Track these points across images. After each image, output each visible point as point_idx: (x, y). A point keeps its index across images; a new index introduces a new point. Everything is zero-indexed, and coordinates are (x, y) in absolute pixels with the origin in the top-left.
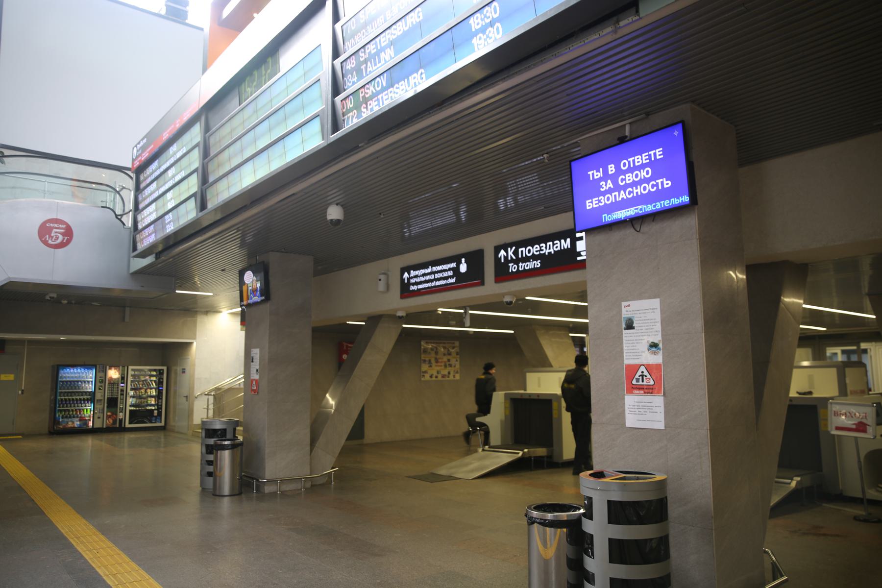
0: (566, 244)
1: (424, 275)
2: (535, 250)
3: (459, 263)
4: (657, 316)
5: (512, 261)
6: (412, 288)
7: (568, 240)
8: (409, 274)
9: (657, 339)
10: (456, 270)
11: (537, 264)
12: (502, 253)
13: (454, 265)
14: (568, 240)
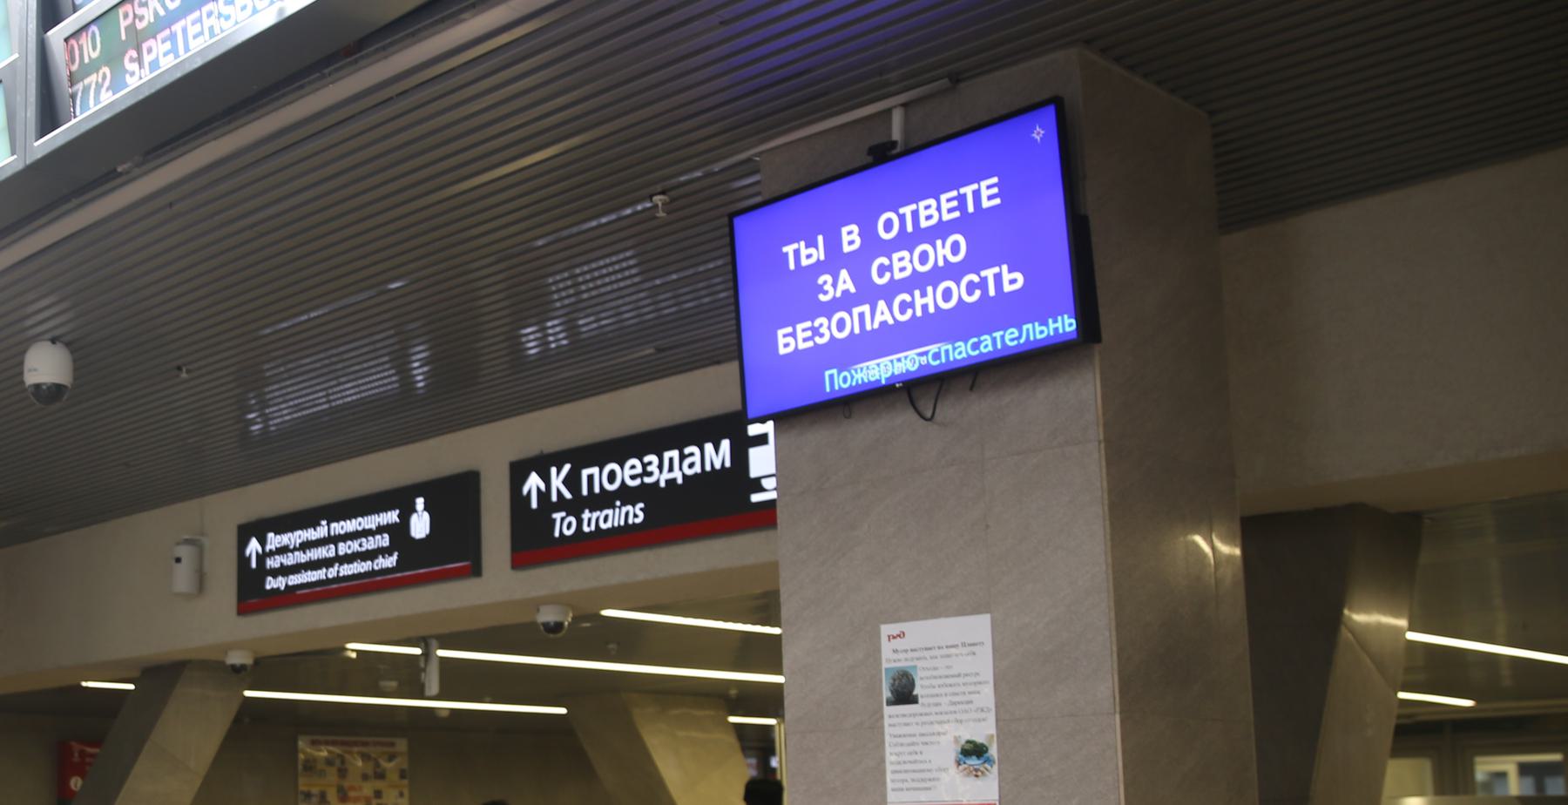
0: (718, 455)
1: (306, 546)
2: (628, 472)
3: (407, 512)
4: (983, 664)
5: (562, 504)
6: (271, 583)
7: (725, 445)
8: (263, 542)
9: (984, 731)
10: (399, 533)
11: (635, 513)
12: (534, 482)
13: (392, 517)
14: (725, 445)
